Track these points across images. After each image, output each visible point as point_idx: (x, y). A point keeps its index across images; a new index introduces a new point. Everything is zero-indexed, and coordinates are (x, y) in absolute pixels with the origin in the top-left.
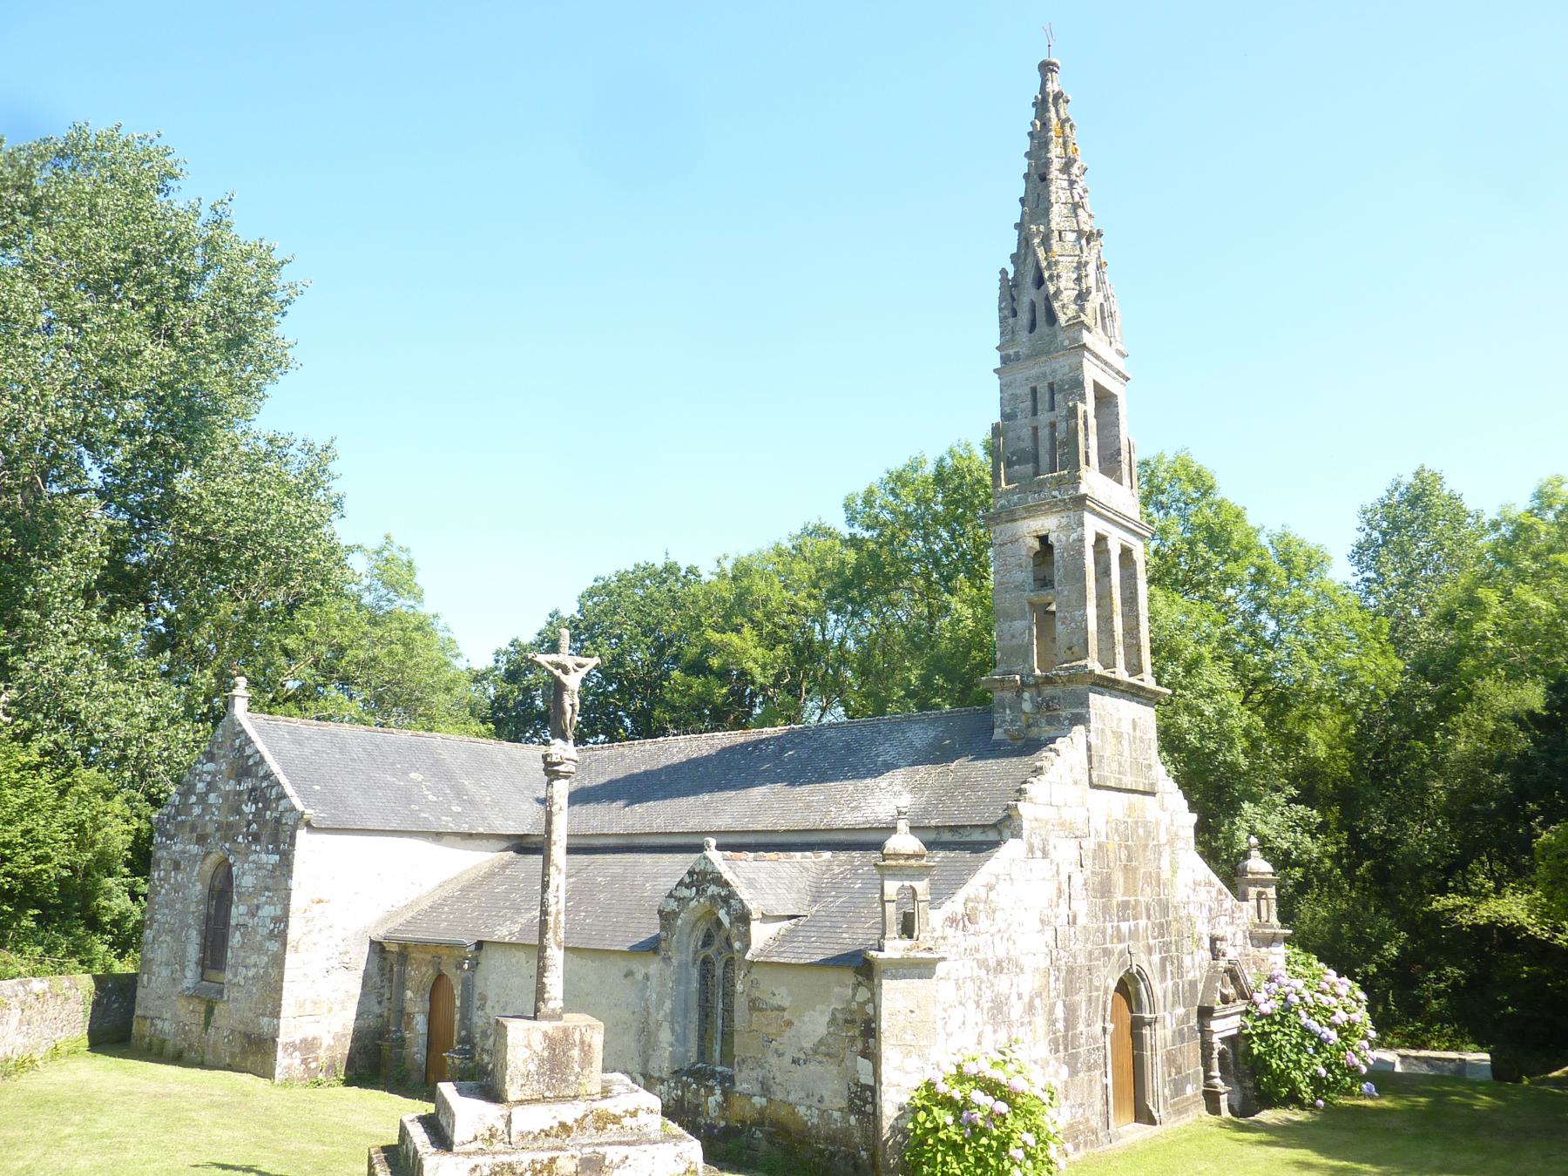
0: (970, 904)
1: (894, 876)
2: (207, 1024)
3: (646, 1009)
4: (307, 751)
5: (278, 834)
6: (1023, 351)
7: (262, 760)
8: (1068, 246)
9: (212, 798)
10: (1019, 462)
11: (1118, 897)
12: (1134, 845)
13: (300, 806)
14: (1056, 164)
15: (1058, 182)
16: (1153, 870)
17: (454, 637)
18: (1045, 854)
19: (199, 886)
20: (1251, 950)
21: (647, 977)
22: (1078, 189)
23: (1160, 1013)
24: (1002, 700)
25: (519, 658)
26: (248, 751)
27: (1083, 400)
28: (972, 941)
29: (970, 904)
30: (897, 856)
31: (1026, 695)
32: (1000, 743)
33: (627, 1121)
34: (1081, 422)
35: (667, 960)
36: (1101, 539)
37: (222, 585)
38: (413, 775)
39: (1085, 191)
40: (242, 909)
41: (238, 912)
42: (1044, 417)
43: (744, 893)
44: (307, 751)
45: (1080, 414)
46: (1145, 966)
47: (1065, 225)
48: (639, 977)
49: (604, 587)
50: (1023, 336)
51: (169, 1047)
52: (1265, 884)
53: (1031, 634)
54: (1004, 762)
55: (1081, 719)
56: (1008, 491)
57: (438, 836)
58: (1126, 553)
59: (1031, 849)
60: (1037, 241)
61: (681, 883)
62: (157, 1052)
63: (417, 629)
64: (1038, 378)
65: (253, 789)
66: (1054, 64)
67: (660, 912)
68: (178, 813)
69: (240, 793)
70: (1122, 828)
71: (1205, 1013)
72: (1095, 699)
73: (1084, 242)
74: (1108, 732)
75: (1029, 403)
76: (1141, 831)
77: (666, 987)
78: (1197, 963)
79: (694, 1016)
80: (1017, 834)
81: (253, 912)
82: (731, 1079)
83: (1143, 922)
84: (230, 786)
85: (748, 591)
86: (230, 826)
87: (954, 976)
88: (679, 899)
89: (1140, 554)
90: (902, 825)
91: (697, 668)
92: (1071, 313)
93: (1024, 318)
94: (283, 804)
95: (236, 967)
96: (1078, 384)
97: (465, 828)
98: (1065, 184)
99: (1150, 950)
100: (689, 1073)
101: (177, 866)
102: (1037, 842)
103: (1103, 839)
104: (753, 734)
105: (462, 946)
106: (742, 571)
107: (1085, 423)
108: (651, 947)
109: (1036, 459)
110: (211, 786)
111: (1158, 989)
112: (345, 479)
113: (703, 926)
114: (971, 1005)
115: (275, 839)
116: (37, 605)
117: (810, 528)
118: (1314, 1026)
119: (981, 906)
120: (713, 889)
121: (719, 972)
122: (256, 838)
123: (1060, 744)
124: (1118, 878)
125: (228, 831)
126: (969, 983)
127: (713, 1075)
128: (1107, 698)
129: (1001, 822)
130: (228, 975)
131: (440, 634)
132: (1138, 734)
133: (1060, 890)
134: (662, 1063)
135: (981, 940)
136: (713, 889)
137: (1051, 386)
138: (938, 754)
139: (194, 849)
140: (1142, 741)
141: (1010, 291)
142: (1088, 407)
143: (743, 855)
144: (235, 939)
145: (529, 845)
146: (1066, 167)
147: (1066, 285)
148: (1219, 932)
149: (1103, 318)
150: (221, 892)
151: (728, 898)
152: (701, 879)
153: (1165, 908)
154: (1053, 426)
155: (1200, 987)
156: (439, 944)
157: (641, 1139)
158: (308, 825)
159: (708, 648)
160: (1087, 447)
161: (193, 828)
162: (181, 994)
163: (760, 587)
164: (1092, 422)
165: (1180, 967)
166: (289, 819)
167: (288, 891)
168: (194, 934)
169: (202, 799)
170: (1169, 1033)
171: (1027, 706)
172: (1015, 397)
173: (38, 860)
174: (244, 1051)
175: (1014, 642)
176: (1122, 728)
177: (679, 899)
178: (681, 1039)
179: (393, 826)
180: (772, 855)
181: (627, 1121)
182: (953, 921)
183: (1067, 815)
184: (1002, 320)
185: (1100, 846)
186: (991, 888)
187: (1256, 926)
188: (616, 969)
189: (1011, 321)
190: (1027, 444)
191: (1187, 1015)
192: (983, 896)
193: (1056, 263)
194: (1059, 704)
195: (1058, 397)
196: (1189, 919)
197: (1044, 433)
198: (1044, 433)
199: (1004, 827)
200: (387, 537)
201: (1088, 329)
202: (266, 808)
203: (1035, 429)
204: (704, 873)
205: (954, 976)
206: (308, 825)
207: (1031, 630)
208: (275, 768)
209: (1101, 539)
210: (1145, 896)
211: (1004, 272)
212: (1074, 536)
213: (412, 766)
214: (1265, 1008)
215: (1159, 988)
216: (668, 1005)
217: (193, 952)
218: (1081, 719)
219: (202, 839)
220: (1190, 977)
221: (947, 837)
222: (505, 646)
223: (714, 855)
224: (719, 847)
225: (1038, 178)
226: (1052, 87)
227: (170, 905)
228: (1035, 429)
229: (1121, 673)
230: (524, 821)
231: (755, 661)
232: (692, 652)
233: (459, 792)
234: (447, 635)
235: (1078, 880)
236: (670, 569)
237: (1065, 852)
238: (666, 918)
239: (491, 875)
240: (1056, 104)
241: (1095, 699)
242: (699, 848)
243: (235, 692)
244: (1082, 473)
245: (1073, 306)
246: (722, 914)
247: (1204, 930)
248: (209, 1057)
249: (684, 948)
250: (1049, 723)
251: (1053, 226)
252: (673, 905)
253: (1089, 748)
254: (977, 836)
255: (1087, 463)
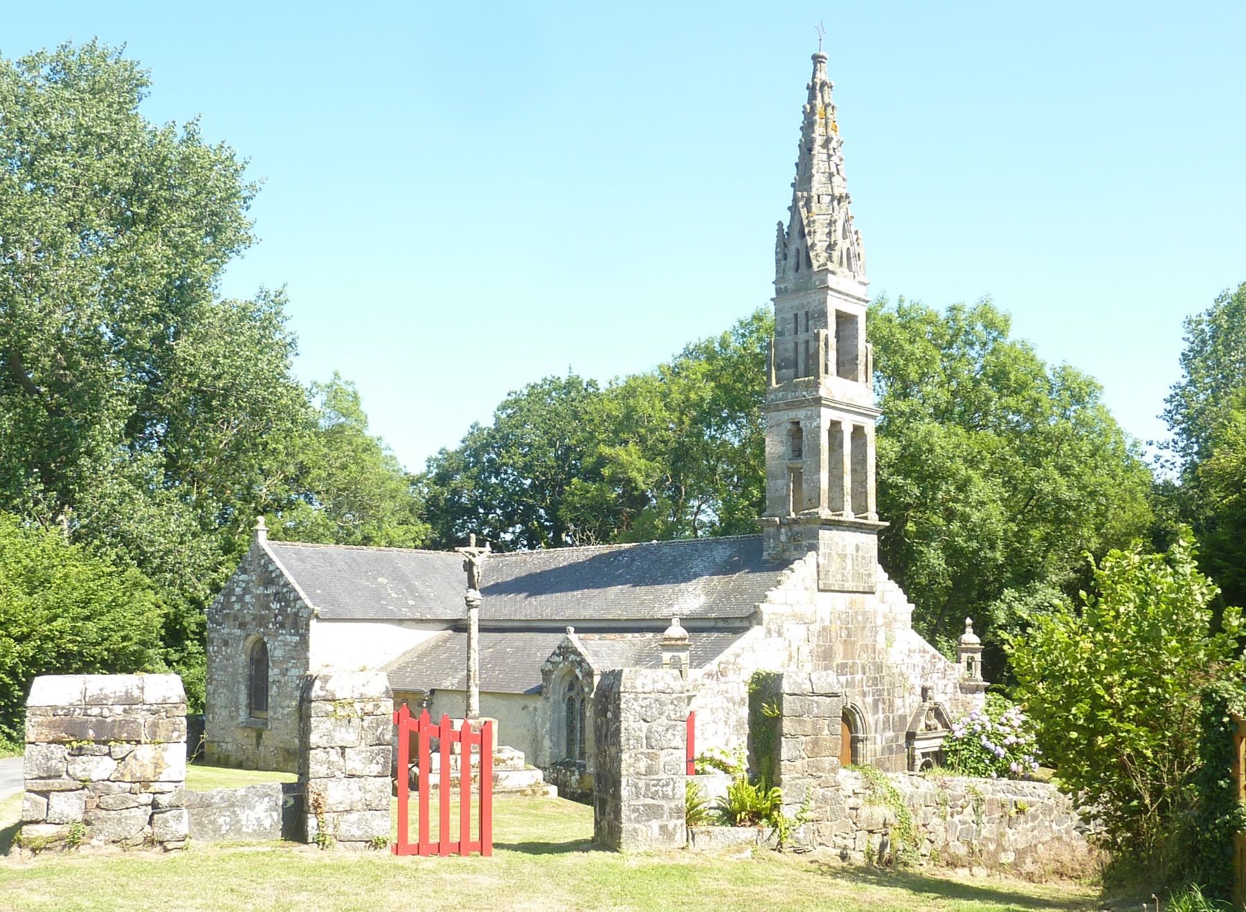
0: (722, 666)
1: (668, 650)
2: (258, 744)
3: (536, 728)
4: (309, 566)
5: (298, 623)
6: (790, 286)
7: (282, 575)
8: (824, 207)
9: (248, 598)
10: (786, 367)
11: (839, 660)
12: (852, 629)
13: (311, 605)
14: (819, 141)
15: (819, 152)
16: (870, 643)
17: (394, 454)
18: (780, 634)
19: (243, 657)
20: (960, 695)
21: (535, 709)
22: (835, 159)
23: (871, 735)
24: (768, 533)
25: (447, 464)
26: (271, 568)
27: (825, 326)
28: (723, 687)
29: (722, 666)
30: (671, 639)
31: (783, 530)
32: (766, 562)
33: (509, 762)
34: (822, 344)
35: (547, 699)
36: (835, 424)
37: (216, 424)
38: (380, 580)
39: (841, 160)
40: (276, 671)
41: (273, 673)
42: (802, 336)
43: (590, 659)
44: (309, 566)
45: (822, 337)
46: (859, 704)
47: (822, 190)
48: (531, 709)
49: (516, 401)
50: (791, 275)
51: (233, 759)
52: (974, 651)
53: (788, 489)
54: (765, 575)
55: (814, 547)
56: (776, 390)
57: (400, 621)
58: (858, 431)
59: (769, 632)
60: (801, 203)
61: (554, 653)
62: (224, 762)
63: (365, 451)
64: (798, 308)
65: (277, 593)
66: (822, 57)
67: (542, 671)
68: (223, 608)
69: (268, 596)
70: (844, 616)
71: (911, 737)
72: (823, 534)
73: (835, 203)
74: (834, 554)
75: (792, 325)
76: (860, 618)
77: (545, 713)
78: (907, 704)
79: (564, 732)
80: (760, 623)
81: (284, 673)
82: (584, 766)
83: (858, 677)
84: (260, 590)
85: (634, 410)
86: (262, 617)
87: (709, 706)
88: (552, 663)
89: (870, 427)
90: (675, 621)
91: (593, 474)
92: (822, 260)
93: (792, 261)
94: (299, 604)
95: (275, 708)
96: (823, 314)
97: (418, 616)
98: (825, 157)
99: (864, 694)
100: (561, 764)
101: (226, 643)
102: (773, 627)
103: (827, 623)
104: (615, 547)
105: (422, 693)
106: (630, 392)
107: (826, 344)
108: (538, 691)
109: (796, 365)
110: (246, 590)
111: (870, 719)
112: (297, 321)
113: (568, 679)
114: (721, 723)
115: (295, 625)
116: (89, 453)
117: (692, 347)
118: (992, 746)
119: (730, 667)
120: (572, 657)
121: (577, 705)
122: (282, 626)
123: (797, 565)
124: (839, 649)
125: (261, 621)
126: (720, 711)
127: (574, 765)
128: (834, 532)
129: (751, 615)
130: (270, 713)
131: (384, 453)
132: (860, 553)
133: (791, 658)
134: (546, 756)
135: (729, 686)
136: (572, 657)
137: (807, 313)
138: (728, 568)
139: (238, 632)
140: (863, 558)
141: (783, 241)
142: (830, 331)
143: (589, 635)
144: (273, 690)
145: (459, 626)
146: (826, 144)
147: (819, 240)
148: (928, 684)
149: (849, 258)
150: (260, 659)
151: (581, 662)
152: (565, 651)
153: (879, 668)
154: (807, 342)
155: (909, 719)
156: (406, 692)
157: (515, 769)
158: (317, 617)
159: (602, 461)
160: (826, 359)
161: (236, 618)
162: (237, 726)
163: (643, 406)
164: (833, 341)
165: (891, 705)
166: (304, 613)
167: (307, 659)
168: (243, 687)
169: (240, 599)
170: (879, 747)
171: (783, 538)
172: (784, 320)
173: (124, 639)
174: (285, 760)
175: (777, 494)
176: (851, 551)
177: (552, 663)
178: (556, 745)
179: (371, 615)
180: (612, 636)
181: (509, 762)
182: (710, 675)
183: (798, 610)
184: (778, 261)
185: (824, 628)
186: (738, 656)
187: (965, 680)
188: (517, 704)
189: (783, 263)
190: (791, 354)
191: (897, 738)
192: (732, 660)
193: (814, 222)
194: (802, 538)
195: (811, 322)
196: (902, 674)
197: (801, 348)
198: (801, 348)
199: (753, 618)
200: (336, 375)
201: (833, 273)
202: (287, 606)
203: (796, 344)
204: (567, 648)
205: (709, 706)
206: (317, 617)
207: (788, 486)
208: (291, 579)
209: (835, 424)
210: (863, 659)
211: (780, 224)
212: (815, 424)
213: (379, 572)
214: (959, 734)
215: (870, 719)
216: (548, 725)
217: (243, 699)
218: (814, 547)
219: (242, 626)
220: (901, 712)
221: (721, 624)
222: (435, 454)
223: (574, 638)
224: (577, 631)
225: (807, 148)
226: (821, 76)
227: (224, 669)
228: (796, 344)
229: (848, 515)
230: (455, 611)
231: (639, 471)
232: (589, 461)
233: (412, 590)
234: (388, 453)
235: (805, 650)
236: (572, 384)
237: (796, 633)
238: (546, 674)
239: (437, 647)
240: (821, 90)
241: (823, 534)
242: (563, 630)
243: (257, 527)
244: (822, 380)
245: (825, 254)
246: (578, 671)
247: (918, 684)
248: (261, 764)
249: (557, 693)
250: (796, 549)
251: (814, 193)
252: (550, 666)
253: (818, 566)
254: (738, 624)
255: (826, 372)
